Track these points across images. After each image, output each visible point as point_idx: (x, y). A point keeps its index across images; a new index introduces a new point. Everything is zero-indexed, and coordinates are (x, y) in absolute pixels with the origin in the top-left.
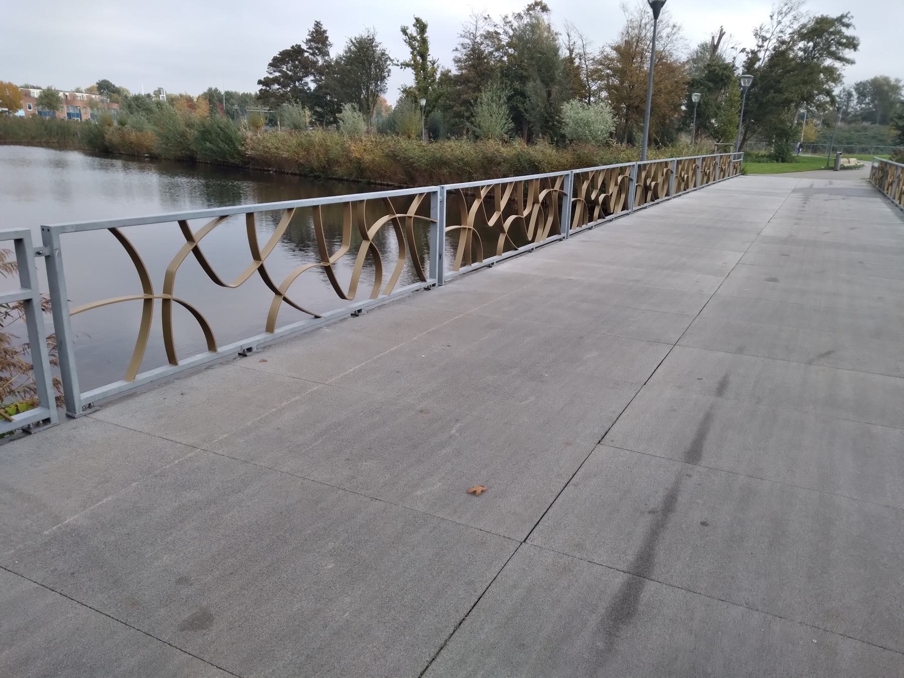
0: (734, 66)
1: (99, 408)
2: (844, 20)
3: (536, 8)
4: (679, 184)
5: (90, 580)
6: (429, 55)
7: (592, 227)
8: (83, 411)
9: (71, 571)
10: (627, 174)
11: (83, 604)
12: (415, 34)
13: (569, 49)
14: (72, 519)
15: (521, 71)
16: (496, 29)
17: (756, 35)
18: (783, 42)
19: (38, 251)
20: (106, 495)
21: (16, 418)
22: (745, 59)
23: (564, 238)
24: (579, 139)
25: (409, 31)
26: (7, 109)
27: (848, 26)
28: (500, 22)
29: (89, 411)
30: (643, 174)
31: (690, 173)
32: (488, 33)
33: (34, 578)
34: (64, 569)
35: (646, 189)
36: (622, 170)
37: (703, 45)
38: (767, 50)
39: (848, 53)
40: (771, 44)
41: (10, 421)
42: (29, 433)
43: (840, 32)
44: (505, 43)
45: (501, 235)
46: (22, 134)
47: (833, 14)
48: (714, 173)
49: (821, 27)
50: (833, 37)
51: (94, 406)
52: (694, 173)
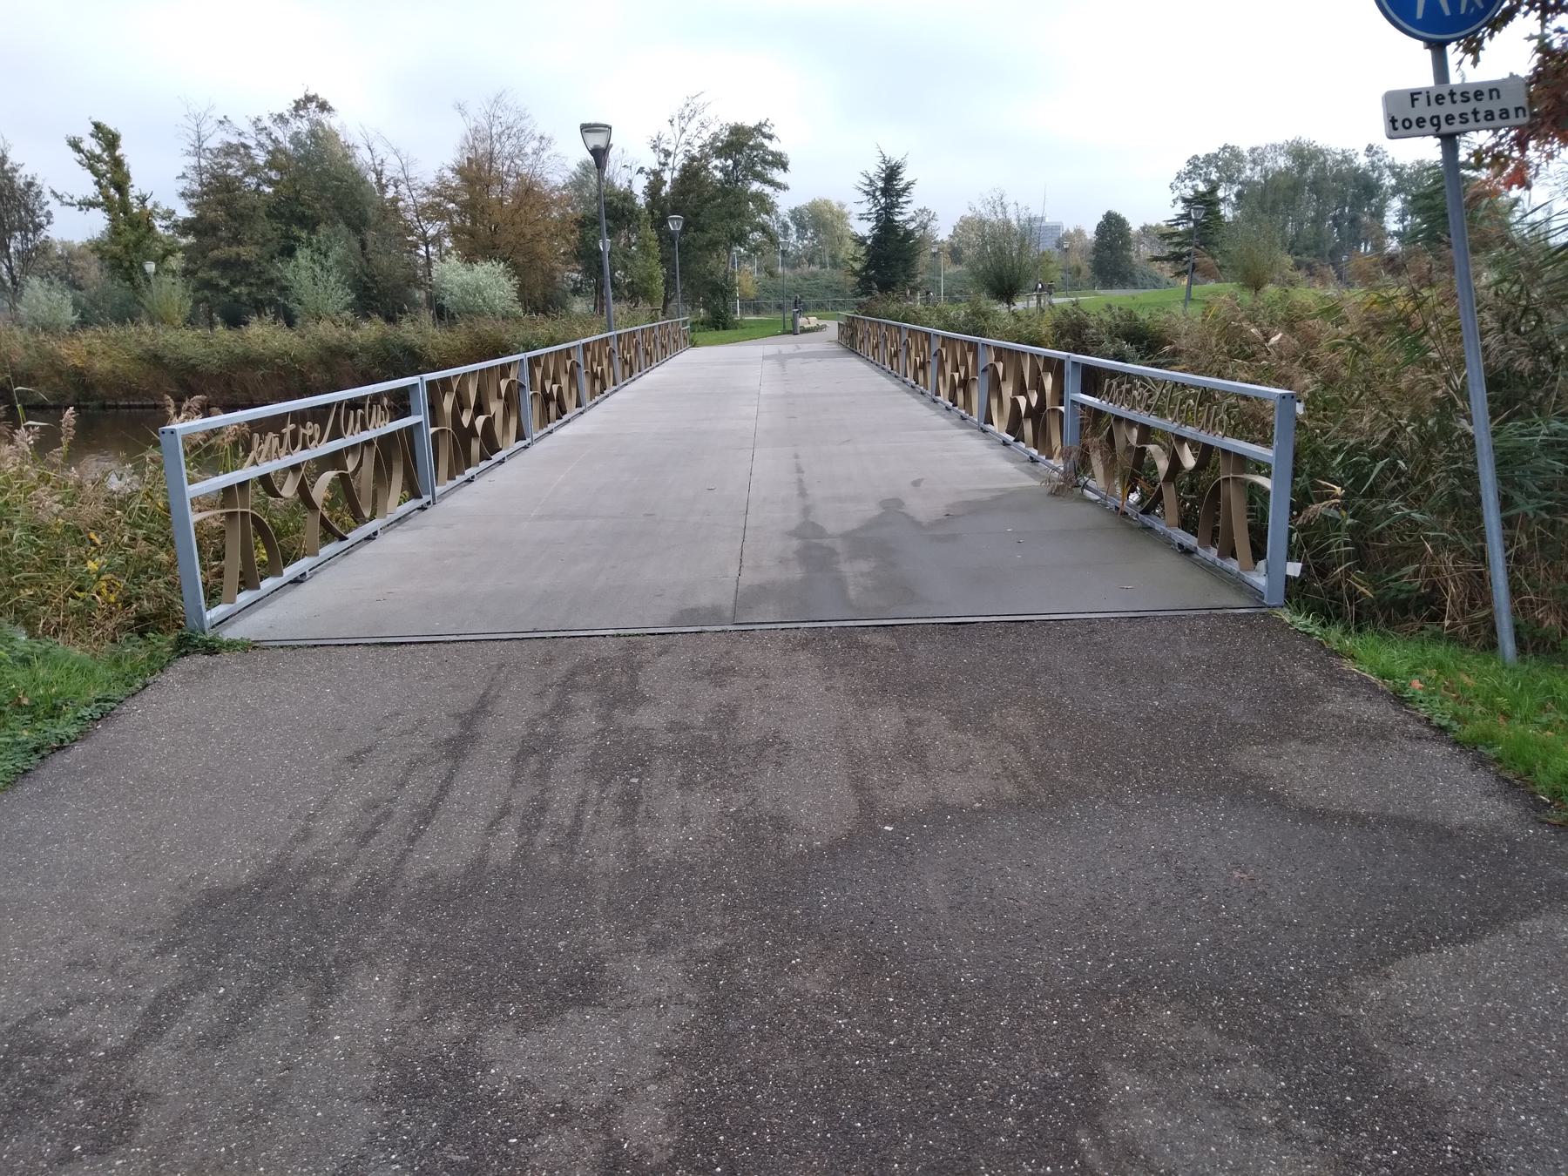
0: (632, 192)
2: (764, 130)
3: (309, 106)
4: (593, 385)
6: (132, 186)
7: (473, 477)
10: (513, 376)
12: (98, 151)
13: (375, 171)
15: (302, 209)
16: (243, 140)
17: (654, 147)
18: (693, 159)
22: (646, 183)
23: (429, 503)
24: (472, 312)
25: (85, 146)
27: (770, 137)
28: (251, 130)
30: (448, 403)
31: (605, 363)
32: (229, 145)
35: (547, 398)
36: (504, 370)
37: (583, 164)
38: (674, 169)
39: (777, 174)
40: (679, 161)
43: (762, 146)
44: (261, 163)
45: (473, 441)
47: (750, 123)
48: (611, 369)
49: (738, 139)
50: (755, 153)
52: (637, 351)
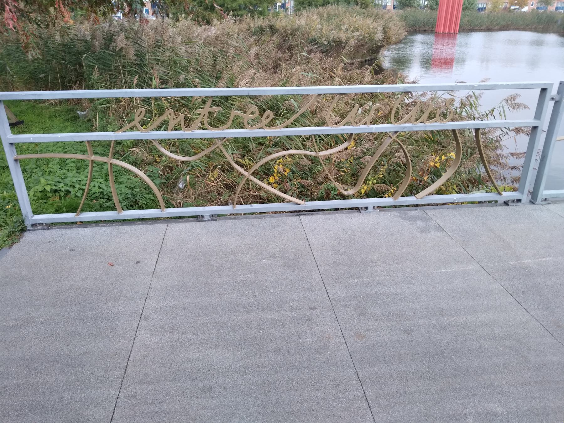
1: (551, 202)
5: (533, 300)
8: (541, 201)
9: (523, 290)
11: (527, 311)
14: (526, 261)
19: (553, 97)
20: (549, 256)
21: (504, 194)
26: (518, 7)
29: (544, 202)
33: (502, 284)
34: (519, 287)
41: (501, 194)
42: (508, 205)
46: (521, 23)
51: (548, 200)
